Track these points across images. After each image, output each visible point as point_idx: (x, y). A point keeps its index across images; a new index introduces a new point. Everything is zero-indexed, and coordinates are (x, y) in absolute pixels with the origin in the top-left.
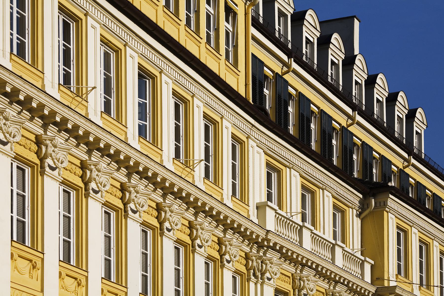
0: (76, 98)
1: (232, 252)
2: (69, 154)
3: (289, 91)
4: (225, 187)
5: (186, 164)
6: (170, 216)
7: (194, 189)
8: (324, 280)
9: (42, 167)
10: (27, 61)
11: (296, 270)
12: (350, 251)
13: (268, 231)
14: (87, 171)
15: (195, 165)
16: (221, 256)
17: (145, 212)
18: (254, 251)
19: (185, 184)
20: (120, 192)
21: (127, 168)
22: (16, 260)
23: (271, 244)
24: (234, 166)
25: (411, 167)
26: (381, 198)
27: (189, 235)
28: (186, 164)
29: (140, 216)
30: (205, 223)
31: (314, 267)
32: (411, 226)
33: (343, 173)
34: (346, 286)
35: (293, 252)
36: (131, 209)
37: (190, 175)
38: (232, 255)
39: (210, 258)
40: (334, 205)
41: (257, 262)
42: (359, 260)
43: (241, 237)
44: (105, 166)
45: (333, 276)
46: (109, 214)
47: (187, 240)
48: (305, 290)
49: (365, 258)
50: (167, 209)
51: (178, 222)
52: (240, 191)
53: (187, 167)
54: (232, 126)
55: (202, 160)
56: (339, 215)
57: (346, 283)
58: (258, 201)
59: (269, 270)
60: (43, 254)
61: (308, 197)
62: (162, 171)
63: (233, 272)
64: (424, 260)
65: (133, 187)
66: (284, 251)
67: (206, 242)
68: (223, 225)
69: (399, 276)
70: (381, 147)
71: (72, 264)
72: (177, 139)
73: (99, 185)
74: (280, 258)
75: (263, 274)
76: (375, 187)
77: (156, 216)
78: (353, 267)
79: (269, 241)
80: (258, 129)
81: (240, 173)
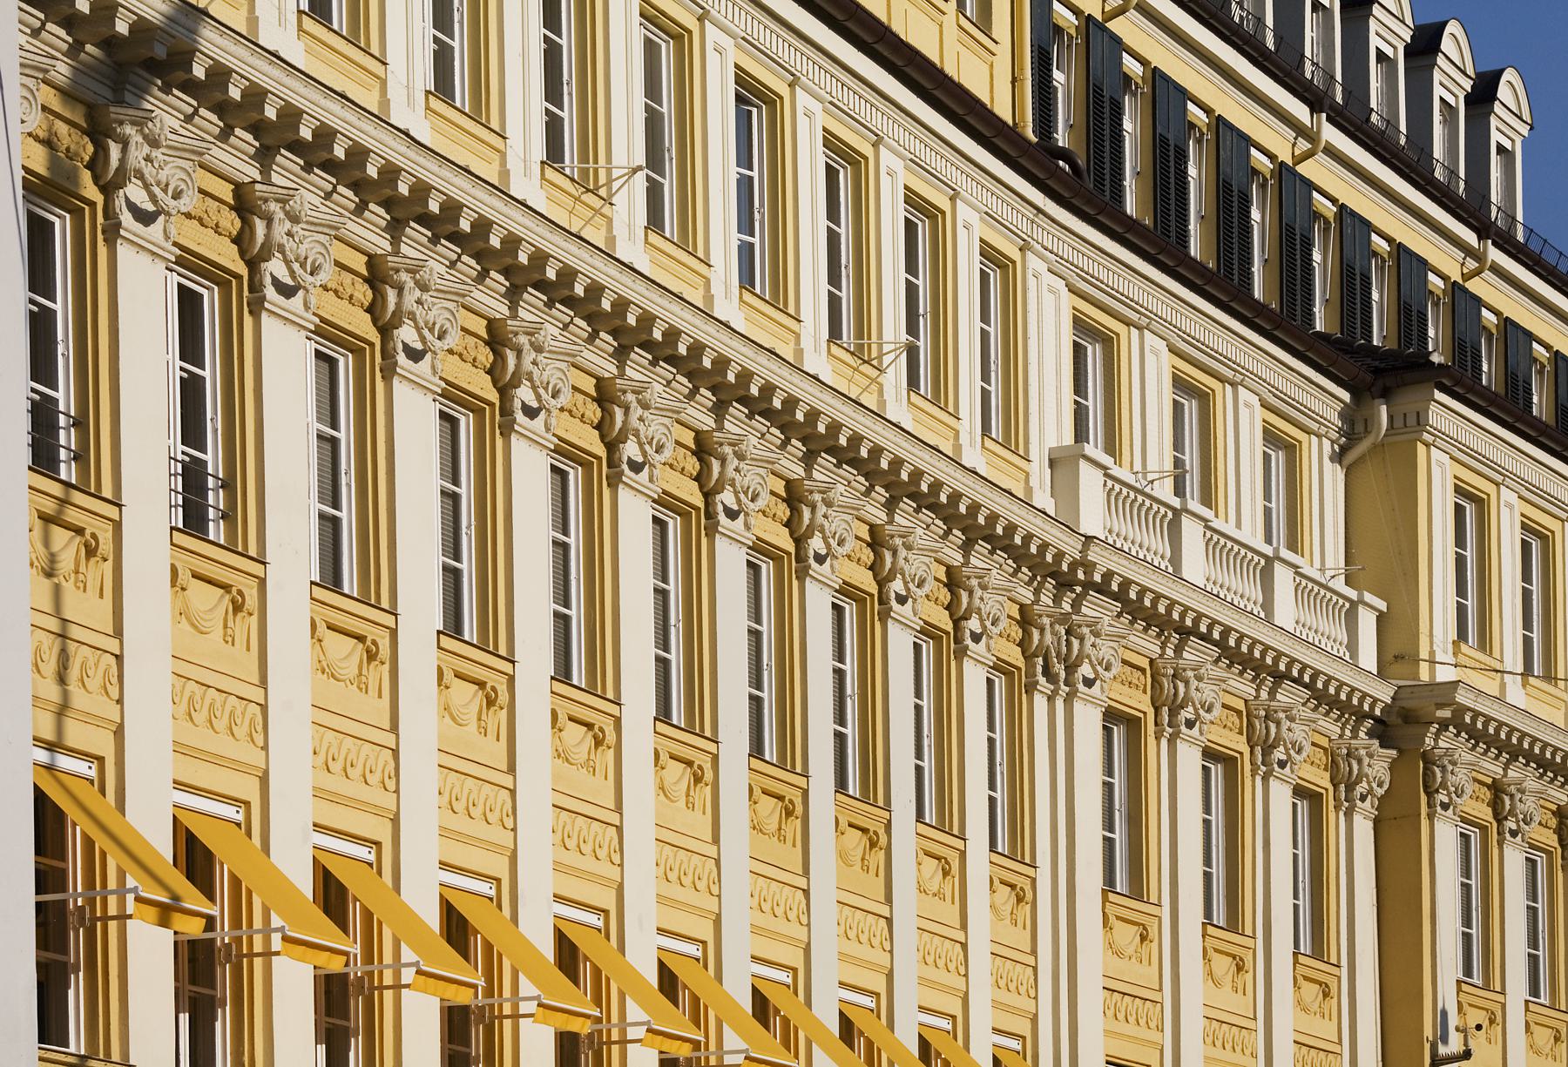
0: (584, 197)
1: (431, 315)
2: (574, 365)
3: (1125, 69)
4: (395, 54)
5: (586, 183)
6: (419, 302)
7: (711, 328)
8: (1241, 673)
9: (506, 411)
10: (458, 104)
11: (1163, 646)
12: (1316, 575)
13: (1089, 539)
14: (257, 221)
15: (616, 185)
16: (956, 623)
17: (325, 288)
18: (1046, 599)
19: (869, 424)
20: (366, 286)
21: (387, 204)
22: (183, 589)
23: (1097, 578)
24: (911, 290)
25: (1487, 274)
26: (1407, 401)
27: (871, 568)
28: (586, 183)
29: (747, 527)
30: (431, 263)
31: (1216, 635)
32: (1497, 484)
33: (1282, 324)
34: (1306, 686)
35: (1158, 597)
36: (132, 207)
37: (597, 218)
38: (650, 443)
39: (847, 590)
40: (1265, 430)
41: (1054, 633)
42: (1341, 601)
43: (1010, 562)
44: (317, 201)
45: (1269, 661)
46: (331, 363)
47: (227, 256)
48: (1190, 709)
49: (1361, 595)
50: (523, 340)
51: (448, 325)
52: (1005, 420)
53: (588, 190)
54: (981, 219)
55: (640, 168)
56: (1279, 458)
57: (1307, 679)
58: (1052, 443)
59: (1088, 657)
60: (120, 506)
61: (1191, 407)
62: (811, 389)
63: (654, 501)
64: (1534, 588)
65: (408, 271)
66: (1133, 595)
67: (439, 338)
68: (713, 389)
69: (1463, 647)
70: (1398, 219)
71: (575, 682)
72: (553, 92)
73: (296, 266)
74: (1119, 615)
75: (1071, 669)
76: (1384, 357)
77: (366, 304)
78: (1324, 625)
79: (1089, 567)
80: (1053, 221)
81: (1004, 358)
